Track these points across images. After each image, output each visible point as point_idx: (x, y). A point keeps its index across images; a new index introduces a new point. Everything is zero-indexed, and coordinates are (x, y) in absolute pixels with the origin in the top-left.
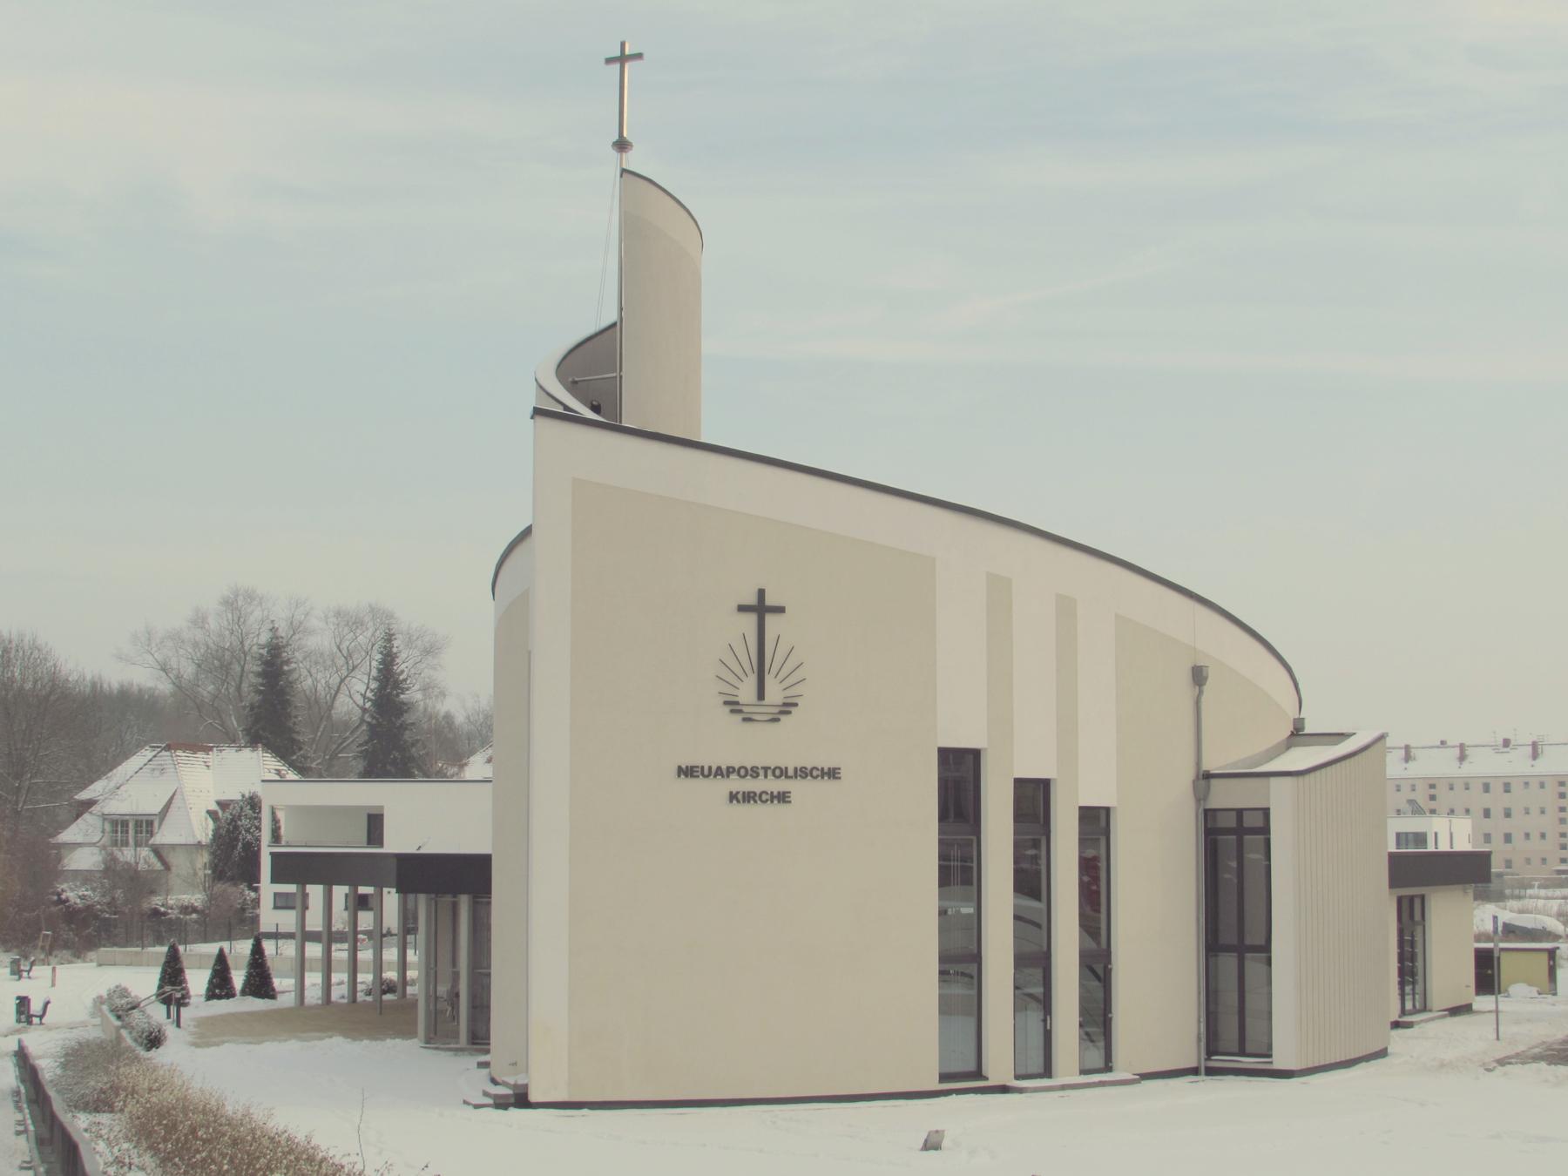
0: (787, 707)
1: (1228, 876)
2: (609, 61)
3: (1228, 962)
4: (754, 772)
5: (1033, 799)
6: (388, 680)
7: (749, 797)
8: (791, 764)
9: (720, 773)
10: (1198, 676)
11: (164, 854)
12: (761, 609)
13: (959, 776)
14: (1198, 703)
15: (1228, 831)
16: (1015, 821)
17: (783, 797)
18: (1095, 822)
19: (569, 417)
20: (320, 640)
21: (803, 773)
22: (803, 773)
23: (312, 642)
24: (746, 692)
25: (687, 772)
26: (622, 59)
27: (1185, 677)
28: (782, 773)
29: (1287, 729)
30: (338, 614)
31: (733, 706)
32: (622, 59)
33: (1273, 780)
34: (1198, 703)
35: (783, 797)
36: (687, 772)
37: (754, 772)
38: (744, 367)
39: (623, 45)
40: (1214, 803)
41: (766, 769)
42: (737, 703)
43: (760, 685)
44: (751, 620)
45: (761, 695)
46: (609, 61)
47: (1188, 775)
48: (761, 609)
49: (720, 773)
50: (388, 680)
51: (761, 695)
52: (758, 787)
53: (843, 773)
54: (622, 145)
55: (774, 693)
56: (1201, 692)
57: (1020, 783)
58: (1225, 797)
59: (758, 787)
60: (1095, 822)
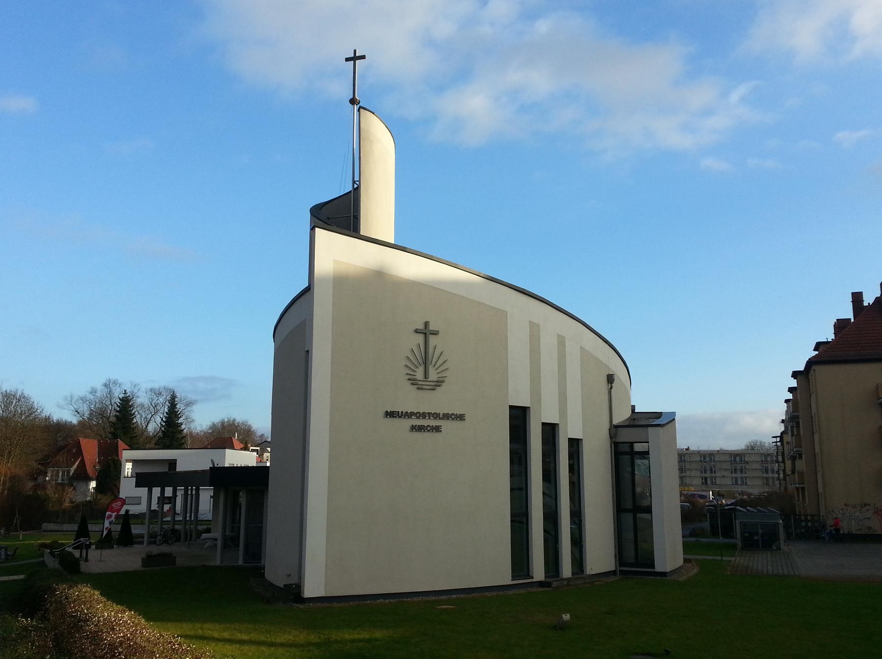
0: (439, 383)
2: (347, 60)
3: (628, 518)
5: (550, 431)
8: (441, 411)
11: (307, 295)
12: (426, 332)
13: (519, 417)
14: (610, 392)
15: (626, 453)
17: (437, 429)
18: (575, 444)
20: (142, 399)
21: (447, 417)
22: (447, 417)
23: (139, 401)
24: (419, 375)
25: (390, 414)
26: (354, 58)
28: (436, 416)
30: (151, 390)
31: (413, 381)
32: (354, 58)
33: (650, 429)
34: (610, 392)
35: (437, 429)
36: (390, 414)
37: (423, 415)
39: (355, 51)
40: (620, 439)
41: (429, 414)
42: (415, 380)
44: (420, 338)
45: (426, 375)
46: (347, 60)
47: (607, 426)
48: (426, 332)
51: (426, 375)
53: (382, 414)
55: (433, 376)
56: (611, 388)
57: (544, 424)
59: (426, 423)
60: (575, 444)
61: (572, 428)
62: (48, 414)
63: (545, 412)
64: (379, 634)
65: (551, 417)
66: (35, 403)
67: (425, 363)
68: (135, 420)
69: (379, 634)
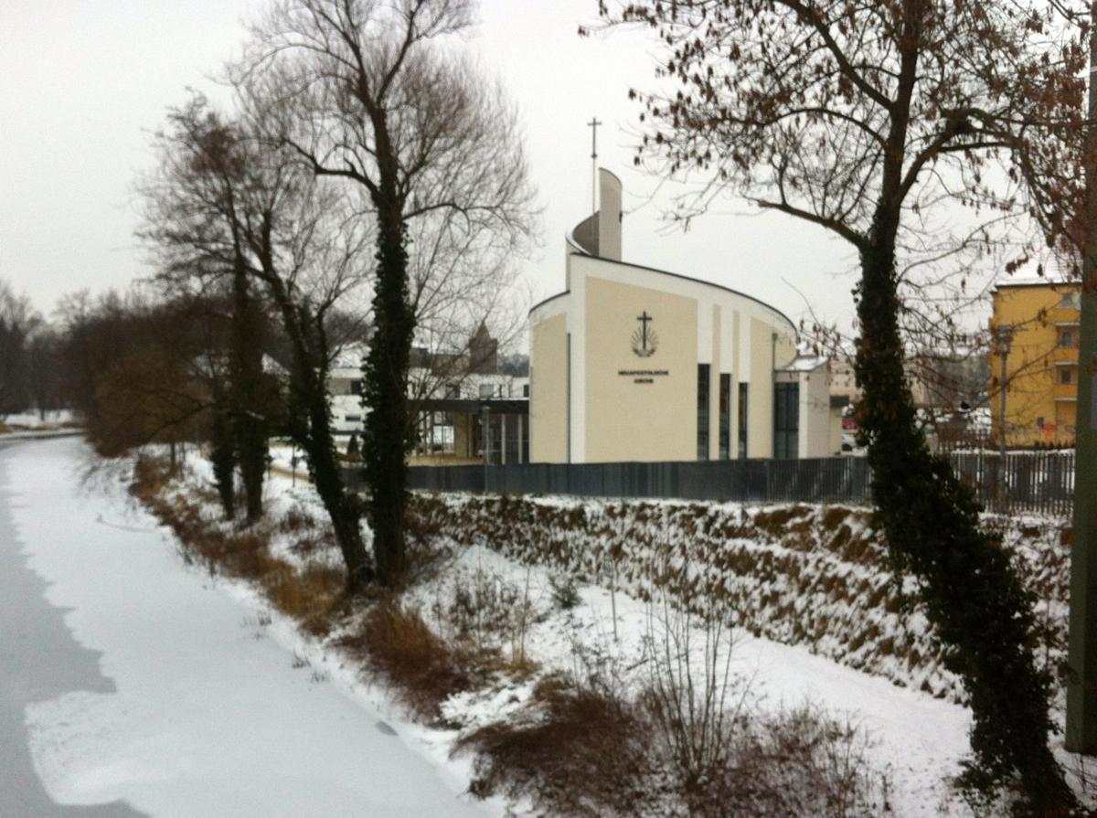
0: (652, 351)
1: (783, 405)
3: (782, 435)
4: (594, 192)
5: (725, 379)
6: (178, 118)
7: (640, 381)
8: (653, 369)
9: (632, 373)
10: (775, 337)
12: (645, 319)
13: (704, 371)
16: (623, 465)
18: (743, 388)
19: (582, 254)
21: (657, 373)
22: (657, 373)
24: (640, 347)
25: (622, 373)
27: (770, 337)
28: (650, 373)
29: (794, 354)
31: (636, 351)
35: (651, 381)
36: (622, 373)
37: (594, 192)
38: (639, 239)
43: (645, 345)
44: (641, 323)
45: (644, 346)
48: (645, 319)
49: (632, 373)
50: (178, 118)
51: (644, 346)
52: (644, 378)
53: (670, 373)
54: (594, 156)
55: (649, 346)
58: (784, 378)
60: (743, 388)
61: (742, 375)
62: (106, 293)
63: (721, 367)
64: (253, 414)
65: (725, 369)
66: (533, 206)
67: (644, 340)
68: (932, 453)
69: (253, 414)
